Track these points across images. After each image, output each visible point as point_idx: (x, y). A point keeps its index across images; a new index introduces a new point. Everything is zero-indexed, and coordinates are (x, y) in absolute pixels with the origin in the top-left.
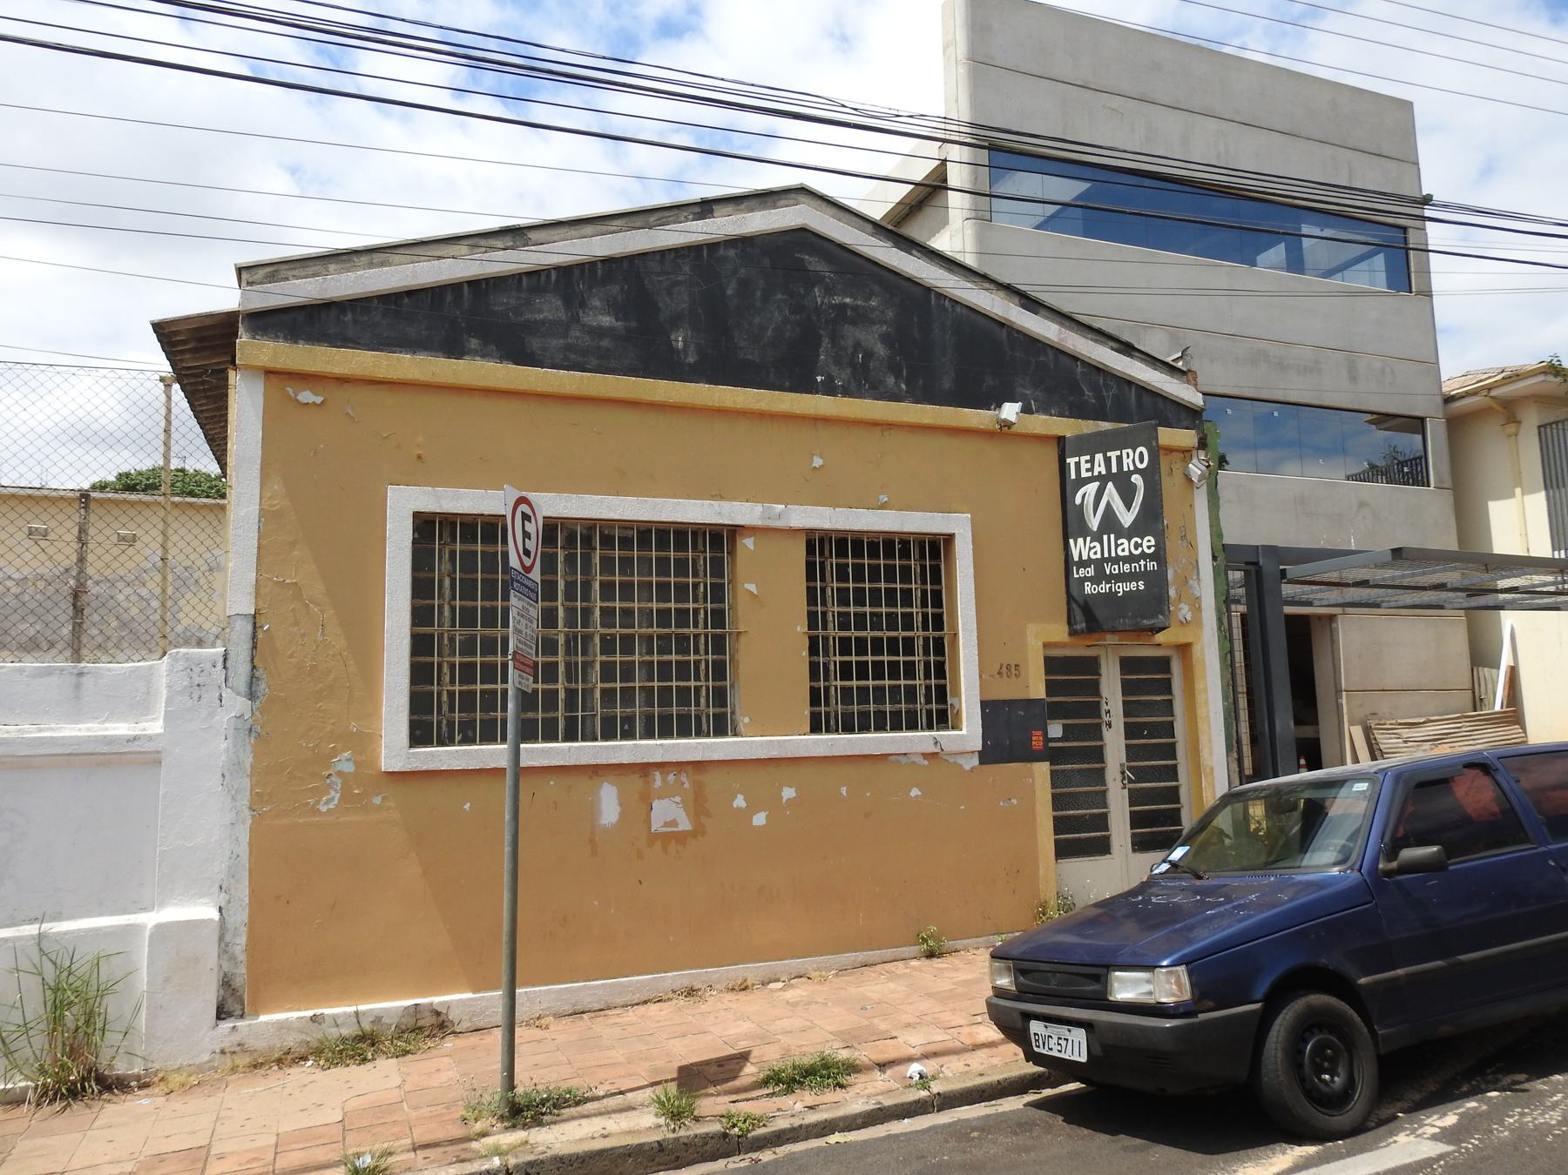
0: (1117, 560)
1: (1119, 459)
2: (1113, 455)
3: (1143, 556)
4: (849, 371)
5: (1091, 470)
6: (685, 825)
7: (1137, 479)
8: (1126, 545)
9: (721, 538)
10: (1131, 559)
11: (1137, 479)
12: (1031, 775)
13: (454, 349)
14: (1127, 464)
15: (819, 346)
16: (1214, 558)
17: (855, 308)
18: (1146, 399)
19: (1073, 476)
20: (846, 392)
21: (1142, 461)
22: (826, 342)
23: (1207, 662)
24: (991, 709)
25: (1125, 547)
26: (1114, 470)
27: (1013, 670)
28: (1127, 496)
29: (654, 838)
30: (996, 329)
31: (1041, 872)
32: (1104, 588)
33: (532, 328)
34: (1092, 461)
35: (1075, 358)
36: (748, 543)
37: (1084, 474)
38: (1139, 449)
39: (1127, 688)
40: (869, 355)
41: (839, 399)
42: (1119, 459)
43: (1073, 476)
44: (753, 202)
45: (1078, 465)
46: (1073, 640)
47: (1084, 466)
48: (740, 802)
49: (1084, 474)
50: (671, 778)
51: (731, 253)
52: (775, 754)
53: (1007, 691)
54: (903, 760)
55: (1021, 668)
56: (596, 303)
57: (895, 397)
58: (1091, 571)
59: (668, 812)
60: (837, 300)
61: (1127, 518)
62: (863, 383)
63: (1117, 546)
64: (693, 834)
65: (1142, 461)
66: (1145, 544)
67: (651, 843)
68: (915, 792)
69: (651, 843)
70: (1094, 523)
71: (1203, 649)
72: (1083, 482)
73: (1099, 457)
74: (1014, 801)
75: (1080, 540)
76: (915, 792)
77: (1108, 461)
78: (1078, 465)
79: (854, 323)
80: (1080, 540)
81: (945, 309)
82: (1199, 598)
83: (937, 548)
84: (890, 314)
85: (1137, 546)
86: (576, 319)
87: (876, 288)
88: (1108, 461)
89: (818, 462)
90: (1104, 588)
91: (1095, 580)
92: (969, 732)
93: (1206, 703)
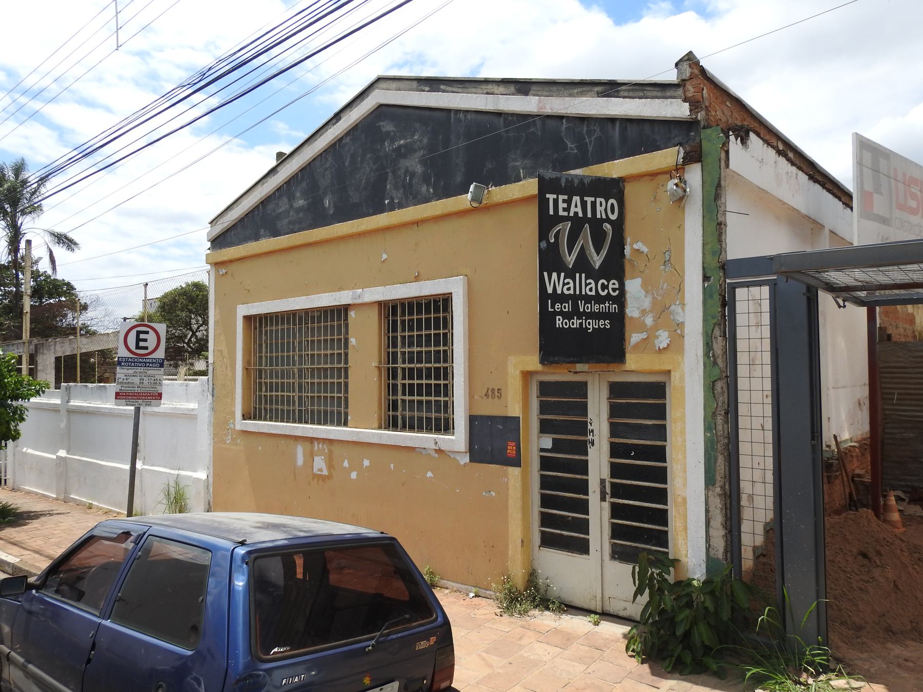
0: (588, 299)
1: (594, 204)
2: (589, 200)
3: (608, 297)
4: (401, 191)
5: (567, 209)
6: (325, 472)
7: (607, 227)
8: (593, 285)
9: (342, 311)
10: (599, 299)
11: (607, 227)
12: (506, 475)
13: (257, 238)
14: (600, 212)
15: (387, 179)
16: (706, 278)
17: (405, 146)
18: (632, 131)
19: (551, 212)
20: (401, 206)
21: (613, 212)
22: (390, 174)
23: (688, 390)
24: (474, 421)
25: (590, 287)
26: (589, 215)
27: (496, 393)
28: (598, 239)
29: (315, 476)
30: (495, 119)
31: (510, 552)
32: (576, 323)
33: (278, 217)
34: (569, 202)
35: (560, 118)
36: (352, 314)
37: (561, 213)
38: (612, 201)
39: (614, 411)
40: (413, 175)
41: (397, 212)
42: (594, 204)
43: (551, 212)
44: (359, 100)
45: (556, 201)
46: (546, 369)
47: (562, 205)
48: (346, 464)
49: (561, 213)
50: (321, 445)
51: (348, 140)
52: (355, 439)
53: (489, 408)
54: (424, 452)
55: (503, 392)
56: (298, 194)
57: (427, 200)
58: (567, 307)
59: (319, 464)
60: (396, 144)
61: (597, 260)
62: (413, 197)
63: (586, 285)
64: (329, 477)
65: (613, 212)
66: (611, 286)
67: (313, 479)
68: (429, 474)
69: (313, 479)
70: (570, 260)
71: (682, 379)
72: (559, 219)
73: (576, 199)
74: (493, 494)
75: (554, 275)
76: (429, 474)
77: (584, 204)
78: (556, 201)
79: (404, 156)
80: (554, 275)
81: (460, 120)
82: (681, 325)
83: (443, 302)
84: (425, 140)
85: (604, 287)
86: (291, 206)
87: (417, 125)
88: (584, 204)
89: (385, 256)
90: (576, 323)
91: (567, 316)
92: (457, 440)
93: (683, 432)
